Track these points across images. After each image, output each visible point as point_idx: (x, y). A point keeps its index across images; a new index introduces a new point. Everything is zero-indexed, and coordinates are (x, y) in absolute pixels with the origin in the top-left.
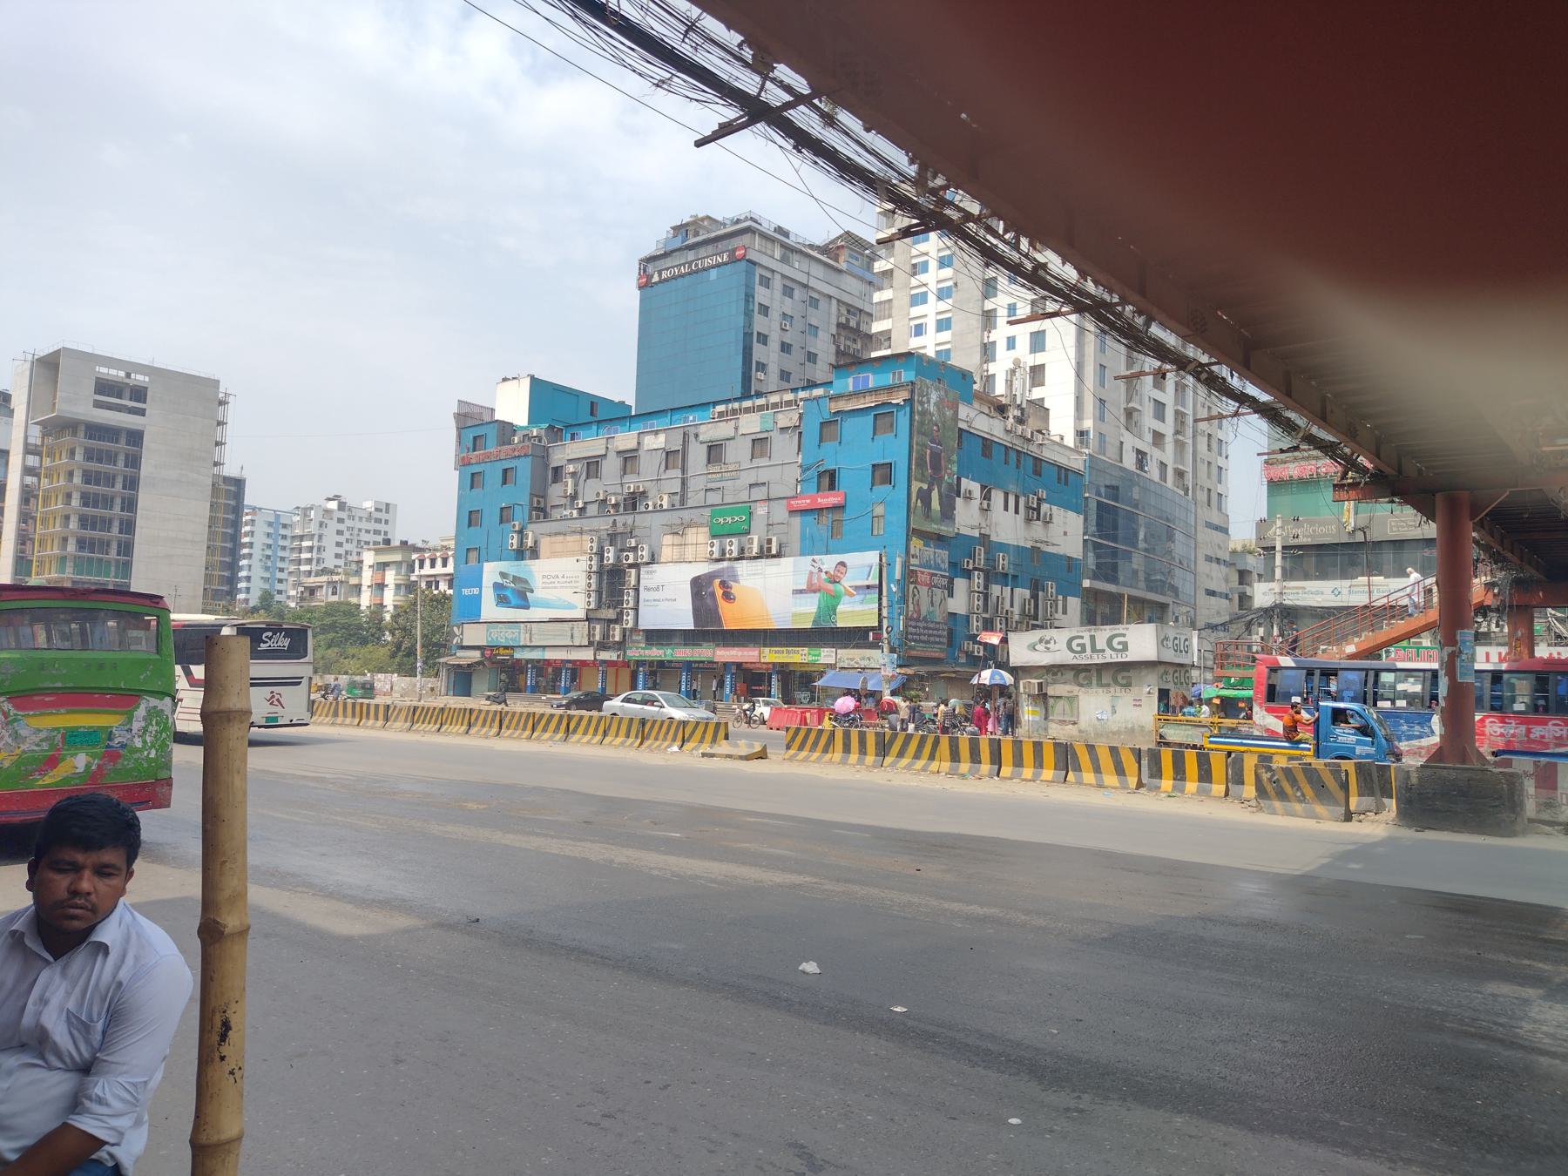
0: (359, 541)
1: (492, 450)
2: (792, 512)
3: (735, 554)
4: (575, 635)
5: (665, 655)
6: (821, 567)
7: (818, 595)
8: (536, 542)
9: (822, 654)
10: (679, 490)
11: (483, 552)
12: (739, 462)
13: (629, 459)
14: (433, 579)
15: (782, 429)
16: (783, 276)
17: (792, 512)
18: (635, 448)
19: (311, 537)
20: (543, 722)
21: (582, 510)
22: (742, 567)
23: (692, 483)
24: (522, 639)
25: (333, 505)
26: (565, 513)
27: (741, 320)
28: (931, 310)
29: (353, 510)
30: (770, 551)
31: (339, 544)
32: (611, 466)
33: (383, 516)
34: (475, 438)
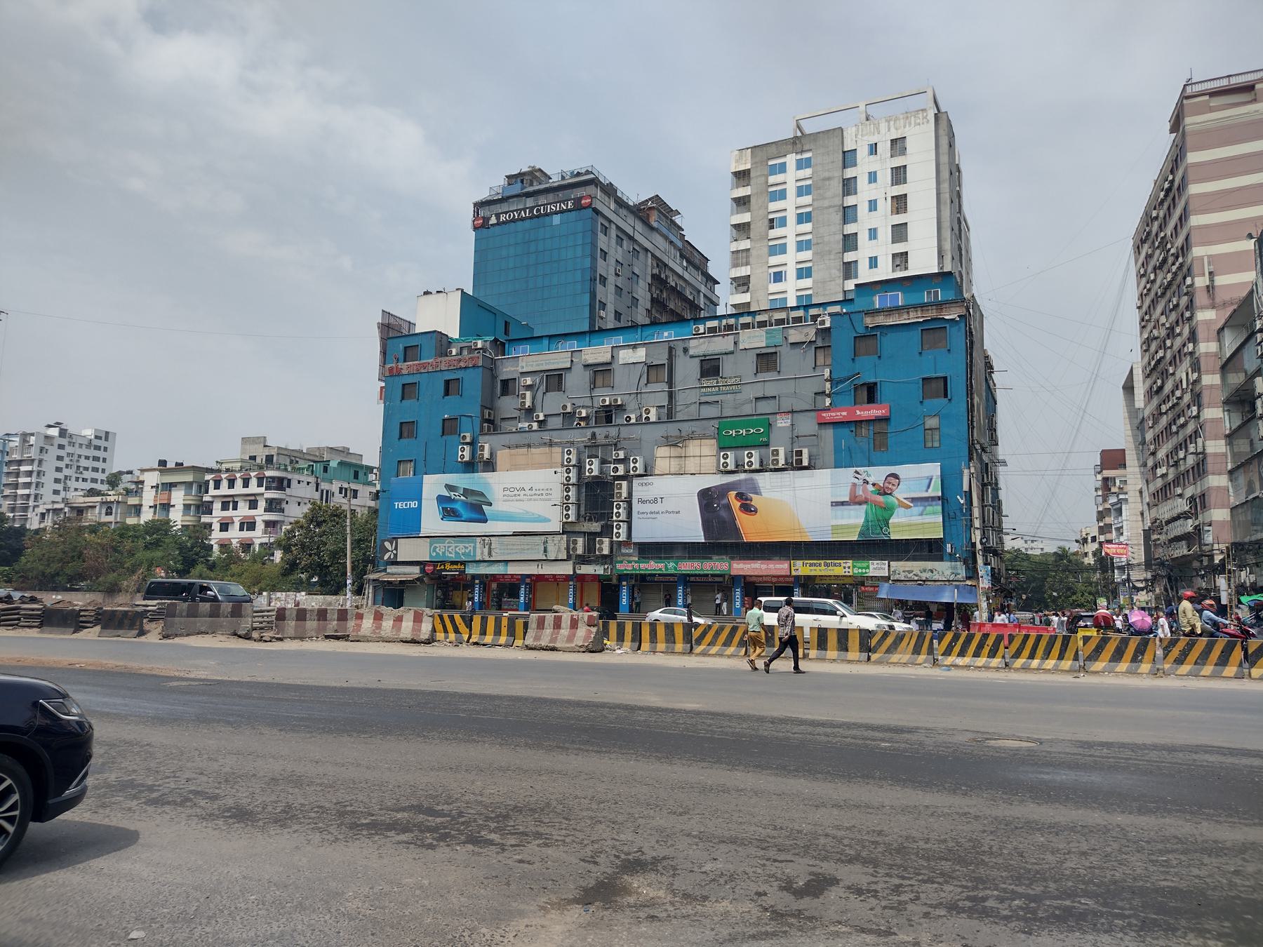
0: (78, 467)
1: (430, 361)
2: (822, 424)
3: (756, 466)
4: (549, 549)
6: (868, 479)
7: (864, 507)
8: (491, 454)
9: (871, 567)
10: (666, 404)
11: (421, 465)
13: (601, 372)
14: (230, 499)
15: (792, 344)
16: (618, 228)
17: (822, 424)
19: (31, 461)
22: (764, 480)
23: (681, 399)
24: (479, 551)
25: (54, 432)
26: (520, 425)
27: (587, 263)
28: (791, 259)
29: (74, 437)
31: (58, 469)
32: (577, 382)
33: (102, 443)
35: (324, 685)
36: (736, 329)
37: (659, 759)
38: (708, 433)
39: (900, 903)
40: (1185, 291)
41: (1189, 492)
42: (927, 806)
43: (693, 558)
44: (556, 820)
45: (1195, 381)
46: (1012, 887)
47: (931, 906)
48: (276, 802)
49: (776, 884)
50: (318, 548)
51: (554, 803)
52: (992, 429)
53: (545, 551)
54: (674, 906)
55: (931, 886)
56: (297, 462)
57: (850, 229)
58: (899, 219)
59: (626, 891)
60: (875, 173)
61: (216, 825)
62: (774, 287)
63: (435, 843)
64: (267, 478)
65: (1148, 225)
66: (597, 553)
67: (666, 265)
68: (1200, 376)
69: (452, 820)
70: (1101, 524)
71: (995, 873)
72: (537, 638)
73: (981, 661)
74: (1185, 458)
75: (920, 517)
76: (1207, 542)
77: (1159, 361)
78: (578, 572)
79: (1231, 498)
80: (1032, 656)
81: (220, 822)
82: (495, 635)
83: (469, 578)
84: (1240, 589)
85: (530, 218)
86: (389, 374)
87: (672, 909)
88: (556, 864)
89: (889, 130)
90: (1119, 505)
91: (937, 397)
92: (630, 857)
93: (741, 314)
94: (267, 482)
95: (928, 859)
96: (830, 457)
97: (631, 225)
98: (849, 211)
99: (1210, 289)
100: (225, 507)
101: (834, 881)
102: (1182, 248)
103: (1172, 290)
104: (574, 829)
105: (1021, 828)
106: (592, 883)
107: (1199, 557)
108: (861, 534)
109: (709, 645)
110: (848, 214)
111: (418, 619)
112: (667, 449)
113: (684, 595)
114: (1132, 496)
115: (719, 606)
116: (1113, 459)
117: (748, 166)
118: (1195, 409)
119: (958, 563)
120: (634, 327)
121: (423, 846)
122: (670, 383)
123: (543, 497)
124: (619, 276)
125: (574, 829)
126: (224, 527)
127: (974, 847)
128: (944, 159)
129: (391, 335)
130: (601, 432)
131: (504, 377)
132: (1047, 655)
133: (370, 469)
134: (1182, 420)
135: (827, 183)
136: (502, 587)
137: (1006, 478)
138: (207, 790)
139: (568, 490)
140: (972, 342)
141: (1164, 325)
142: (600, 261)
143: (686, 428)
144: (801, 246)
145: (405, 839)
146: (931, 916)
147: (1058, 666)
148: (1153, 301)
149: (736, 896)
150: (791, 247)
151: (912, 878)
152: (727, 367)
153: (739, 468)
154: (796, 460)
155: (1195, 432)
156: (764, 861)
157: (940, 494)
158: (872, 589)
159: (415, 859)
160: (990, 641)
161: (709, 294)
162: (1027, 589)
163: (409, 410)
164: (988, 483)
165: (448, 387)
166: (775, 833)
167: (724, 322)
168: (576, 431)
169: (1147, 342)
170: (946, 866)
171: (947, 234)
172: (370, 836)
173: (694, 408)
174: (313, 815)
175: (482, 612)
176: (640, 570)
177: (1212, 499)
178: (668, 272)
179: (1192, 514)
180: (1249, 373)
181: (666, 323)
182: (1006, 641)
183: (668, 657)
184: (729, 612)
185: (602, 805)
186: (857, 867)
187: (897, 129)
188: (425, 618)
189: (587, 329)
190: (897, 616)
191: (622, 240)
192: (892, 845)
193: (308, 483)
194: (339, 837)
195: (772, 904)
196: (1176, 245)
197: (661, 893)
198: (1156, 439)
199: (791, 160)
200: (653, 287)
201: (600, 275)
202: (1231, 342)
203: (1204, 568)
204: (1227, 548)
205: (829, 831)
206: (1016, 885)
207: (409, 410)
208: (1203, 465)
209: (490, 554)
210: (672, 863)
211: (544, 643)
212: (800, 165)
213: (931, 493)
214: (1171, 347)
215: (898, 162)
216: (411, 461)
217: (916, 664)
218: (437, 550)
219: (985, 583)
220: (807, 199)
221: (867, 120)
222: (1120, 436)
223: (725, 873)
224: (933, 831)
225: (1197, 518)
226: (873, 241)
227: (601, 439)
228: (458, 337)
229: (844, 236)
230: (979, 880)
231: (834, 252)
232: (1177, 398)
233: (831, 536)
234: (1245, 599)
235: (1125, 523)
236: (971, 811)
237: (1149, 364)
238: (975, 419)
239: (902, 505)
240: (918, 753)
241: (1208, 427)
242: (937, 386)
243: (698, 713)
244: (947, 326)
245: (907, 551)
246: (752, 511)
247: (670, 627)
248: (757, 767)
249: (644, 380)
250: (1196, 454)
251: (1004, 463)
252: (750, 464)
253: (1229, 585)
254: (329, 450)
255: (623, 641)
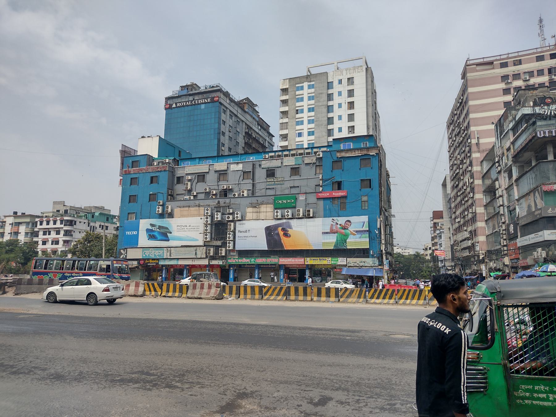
1: (144, 168)
2: (318, 199)
3: (290, 216)
4: (198, 253)
5: (251, 262)
6: (338, 222)
7: (336, 234)
8: (172, 210)
9: (339, 260)
10: (251, 189)
11: (139, 215)
12: (284, 177)
13: (222, 174)
14: (47, 230)
15: (305, 164)
16: (230, 111)
17: (318, 199)
18: (226, 169)
20: (348, 293)
21: (195, 196)
22: (294, 222)
23: (258, 187)
24: (165, 254)
26: (185, 197)
27: (217, 126)
28: (305, 127)
30: (310, 215)
32: (211, 178)
34: (133, 162)
35: (93, 316)
36: (282, 157)
37: (251, 347)
38: (270, 202)
39: (359, 407)
40: (468, 145)
41: (470, 229)
42: (368, 364)
43: (263, 257)
44: (206, 376)
45: (472, 183)
46: (406, 399)
47: (372, 408)
48: (75, 371)
49: (306, 401)
50: (89, 253)
51: (205, 368)
52: (389, 201)
53: (196, 254)
54: (261, 412)
55: (372, 399)
56: (79, 213)
57: (330, 115)
58: (351, 112)
59: (240, 406)
60: (341, 92)
61: (46, 383)
62: (298, 139)
63: (151, 388)
64: (65, 220)
65: (453, 117)
66: (219, 255)
67: (251, 128)
68: (474, 180)
69: (158, 378)
70: (433, 242)
71: (398, 393)
72: (193, 293)
73: (386, 301)
74: (468, 215)
75: (360, 239)
76: (477, 250)
77: (457, 174)
78: (211, 263)
79: (487, 232)
80: (407, 299)
81: (48, 381)
82: (173, 292)
83: (160, 266)
84: (490, 270)
85: (191, 105)
86: (124, 173)
87: (260, 414)
88: (208, 396)
89: (347, 74)
90: (440, 234)
91: (367, 188)
92: (241, 391)
93: (284, 151)
94: (65, 222)
95: (370, 388)
96: (322, 213)
97: (236, 110)
98: (330, 108)
99: (478, 144)
100: (45, 234)
101: (330, 399)
102: (467, 127)
103: (462, 144)
104: (215, 380)
105: (408, 373)
106: (224, 404)
107: (473, 256)
108: (335, 246)
109: (270, 295)
110: (330, 109)
111: (137, 285)
112: (252, 208)
113: (258, 273)
114: (446, 230)
115: (273, 279)
116: (437, 215)
117: (287, 87)
118: (471, 194)
119: (375, 259)
120: (237, 154)
121: (146, 389)
122: (253, 179)
123: (195, 230)
124: (230, 132)
125: (215, 380)
126: (44, 243)
127: (389, 382)
128: (370, 87)
129: (126, 156)
130: (222, 201)
131: (178, 176)
132: (413, 298)
133: (114, 217)
134: (466, 199)
135: (321, 95)
136: (175, 270)
137: (395, 222)
138: (40, 366)
139: (206, 227)
140: (381, 165)
141: (459, 159)
142: (222, 125)
143: (260, 199)
144: (310, 122)
145: (137, 386)
146: (373, 412)
147: (418, 303)
148: (454, 149)
149: (289, 407)
150: (306, 122)
151: (364, 396)
152: (278, 173)
153: (283, 217)
154: (307, 214)
155: (472, 204)
156: (300, 391)
157: (368, 229)
158: (339, 270)
159: (142, 395)
160: (390, 292)
161: (270, 141)
162: (403, 269)
163: (134, 190)
164: (388, 225)
165: (152, 180)
166: (304, 378)
167: (277, 154)
168: (211, 200)
169: (452, 166)
170: (378, 390)
171: (371, 119)
172: (120, 385)
173: (264, 191)
174: (93, 376)
175: (167, 282)
176: (239, 262)
177: (479, 232)
178: (252, 131)
179: (471, 238)
180: (493, 180)
181: (251, 153)
182: (396, 292)
183: (252, 301)
184: (278, 281)
185: (227, 369)
186: (340, 392)
187: (350, 74)
188: (141, 285)
189: (216, 155)
190: (350, 282)
191: (232, 116)
192: (354, 382)
193: (84, 223)
194: (107, 386)
195: (305, 410)
196: (464, 126)
197: (255, 407)
198: (456, 207)
199: (306, 85)
200: (246, 138)
201: (222, 131)
202: (486, 166)
203: (476, 261)
204: (485, 252)
205: (327, 376)
206: (408, 398)
207: (134, 190)
208: (475, 218)
209: (170, 255)
210: (260, 393)
211: (196, 296)
212: (310, 87)
213: (365, 229)
214: (462, 168)
215: (350, 88)
216: (134, 213)
217: (359, 303)
218: (146, 254)
219: (386, 267)
220: (312, 102)
221: (338, 69)
222: (440, 206)
223: (283, 397)
224: (371, 375)
225: (473, 240)
226: (340, 121)
227: (222, 204)
228: (157, 157)
229: (328, 118)
230: (391, 396)
231: (324, 125)
232: (464, 190)
233: (322, 247)
234: (492, 274)
235: (443, 242)
236: (386, 366)
237: (453, 175)
238: (382, 197)
239: (352, 234)
240: (362, 341)
241: (477, 202)
242: (367, 183)
243: (267, 326)
244: (371, 157)
245: (354, 254)
246: (288, 236)
247: (253, 288)
248: (294, 349)
249: (242, 178)
250: (472, 213)
251: (394, 216)
252: (288, 216)
253: (486, 268)
254: (95, 208)
255: (232, 294)
